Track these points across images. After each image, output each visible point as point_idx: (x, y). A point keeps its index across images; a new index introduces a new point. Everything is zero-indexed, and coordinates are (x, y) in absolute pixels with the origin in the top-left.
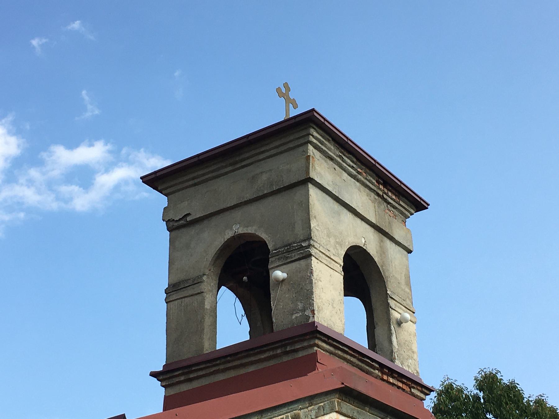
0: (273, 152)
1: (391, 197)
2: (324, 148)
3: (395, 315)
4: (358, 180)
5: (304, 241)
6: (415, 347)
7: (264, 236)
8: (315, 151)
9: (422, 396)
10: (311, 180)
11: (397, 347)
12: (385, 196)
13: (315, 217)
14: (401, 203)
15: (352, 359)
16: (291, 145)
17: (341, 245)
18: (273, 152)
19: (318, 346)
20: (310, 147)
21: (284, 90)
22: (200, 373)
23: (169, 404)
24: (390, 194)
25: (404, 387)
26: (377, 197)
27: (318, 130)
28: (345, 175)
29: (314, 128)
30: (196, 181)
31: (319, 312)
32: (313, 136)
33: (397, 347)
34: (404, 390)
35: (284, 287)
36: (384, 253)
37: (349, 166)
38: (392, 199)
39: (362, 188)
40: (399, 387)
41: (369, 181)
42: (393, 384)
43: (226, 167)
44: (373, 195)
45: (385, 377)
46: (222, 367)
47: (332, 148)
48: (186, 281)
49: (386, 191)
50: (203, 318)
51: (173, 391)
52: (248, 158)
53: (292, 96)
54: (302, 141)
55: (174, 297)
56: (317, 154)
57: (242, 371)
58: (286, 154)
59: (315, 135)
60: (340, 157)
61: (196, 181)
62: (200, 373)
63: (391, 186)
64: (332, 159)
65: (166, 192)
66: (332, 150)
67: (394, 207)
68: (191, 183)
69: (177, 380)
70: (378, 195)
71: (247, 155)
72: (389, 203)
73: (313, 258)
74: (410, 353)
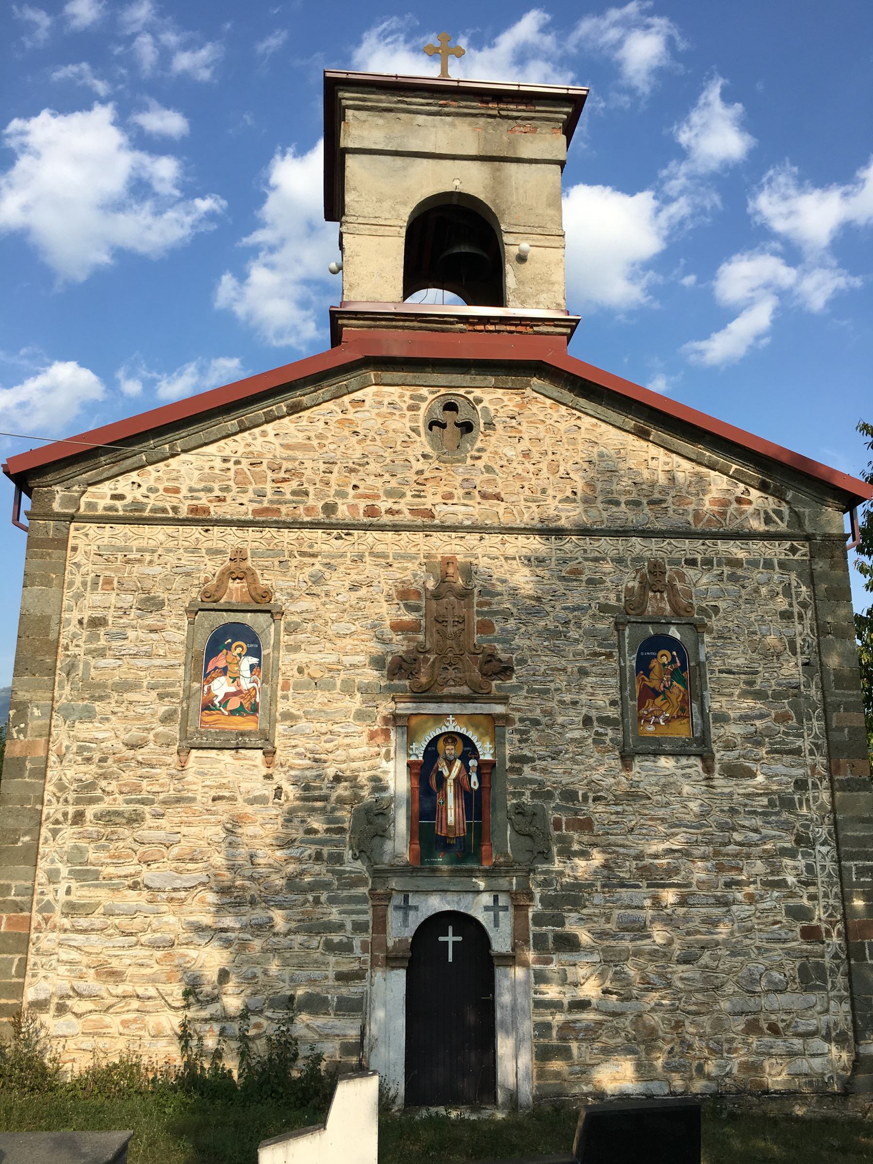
2: (369, 104)
4: (448, 115)
8: (357, 113)
12: (503, 113)
14: (538, 108)
19: (346, 326)
24: (512, 107)
26: (490, 120)
27: (349, 88)
28: (421, 119)
29: (342, 90)
32: (344, 98)
34: (520, 332)
37: (422, 105)
39: (458, 121)
44: (482, 121)
59: (347, 97)
64: (390, 110)
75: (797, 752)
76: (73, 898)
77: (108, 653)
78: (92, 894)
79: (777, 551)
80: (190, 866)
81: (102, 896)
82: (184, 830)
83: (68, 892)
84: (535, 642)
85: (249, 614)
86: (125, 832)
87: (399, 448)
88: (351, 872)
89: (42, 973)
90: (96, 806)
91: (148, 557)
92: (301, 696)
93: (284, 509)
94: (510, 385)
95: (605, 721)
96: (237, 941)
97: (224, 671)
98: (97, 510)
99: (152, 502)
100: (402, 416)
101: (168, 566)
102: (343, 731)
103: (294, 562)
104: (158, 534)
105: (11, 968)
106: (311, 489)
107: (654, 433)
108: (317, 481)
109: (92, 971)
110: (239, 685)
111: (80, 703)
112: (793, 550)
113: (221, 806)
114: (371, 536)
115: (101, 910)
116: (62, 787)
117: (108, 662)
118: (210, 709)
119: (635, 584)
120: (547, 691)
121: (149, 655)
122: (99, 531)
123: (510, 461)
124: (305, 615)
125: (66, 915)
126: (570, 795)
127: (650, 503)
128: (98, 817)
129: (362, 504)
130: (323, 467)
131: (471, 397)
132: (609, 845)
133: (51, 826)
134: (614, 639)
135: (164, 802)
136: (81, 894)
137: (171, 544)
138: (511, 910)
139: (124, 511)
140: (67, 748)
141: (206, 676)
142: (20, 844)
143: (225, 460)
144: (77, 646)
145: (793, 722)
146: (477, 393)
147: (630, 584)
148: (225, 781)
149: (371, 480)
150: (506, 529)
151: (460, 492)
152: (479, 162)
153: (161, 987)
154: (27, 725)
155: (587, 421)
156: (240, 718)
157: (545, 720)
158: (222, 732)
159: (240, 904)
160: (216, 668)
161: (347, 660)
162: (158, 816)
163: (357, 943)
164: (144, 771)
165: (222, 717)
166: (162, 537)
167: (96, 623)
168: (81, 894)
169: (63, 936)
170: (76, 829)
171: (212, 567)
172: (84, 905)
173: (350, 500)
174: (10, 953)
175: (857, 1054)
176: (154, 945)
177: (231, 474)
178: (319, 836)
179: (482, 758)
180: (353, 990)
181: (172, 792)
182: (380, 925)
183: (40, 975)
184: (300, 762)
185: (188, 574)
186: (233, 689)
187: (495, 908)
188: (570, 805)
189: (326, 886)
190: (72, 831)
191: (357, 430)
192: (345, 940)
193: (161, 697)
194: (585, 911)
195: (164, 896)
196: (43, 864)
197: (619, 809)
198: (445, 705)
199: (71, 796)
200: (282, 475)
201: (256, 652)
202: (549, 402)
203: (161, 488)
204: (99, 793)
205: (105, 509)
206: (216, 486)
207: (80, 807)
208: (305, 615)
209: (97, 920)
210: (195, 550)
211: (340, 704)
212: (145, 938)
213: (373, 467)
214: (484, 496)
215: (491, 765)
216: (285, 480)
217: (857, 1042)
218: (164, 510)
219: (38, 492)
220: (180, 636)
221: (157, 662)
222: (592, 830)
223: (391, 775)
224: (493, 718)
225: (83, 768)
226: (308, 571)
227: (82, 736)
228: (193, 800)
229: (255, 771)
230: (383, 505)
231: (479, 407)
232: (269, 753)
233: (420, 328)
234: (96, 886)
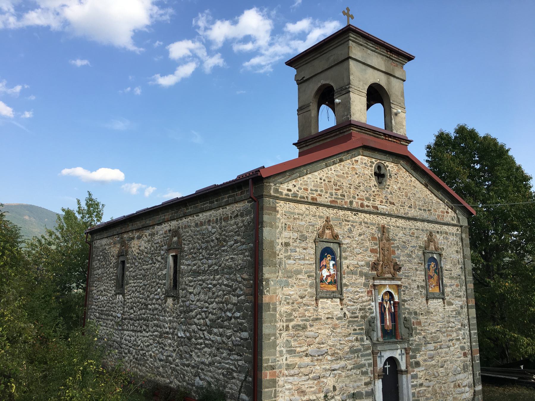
0: (335, 46)
1: (394, 57)
2: (357, 41)
3: (394, 111)
4: (376, 52)
5: (347, 85)
6: (404, 124)
7: (332, 84)
8: (353, 43)
9: (407, 144)
10: (350, 58)
11: (394, 125)
12: (391, 57)
13: (352, 74)
15: (370, 133)
16: (342, 42)
17: (366, 84)
18: (335, 46)
19: (353, 130)
20: (350, 42)
21: (346, 11)
22: (310, 143)
23: (300, 154)
24: (394, 55)
25: (397, 141)
26: (387, 58)
28: (369, 51)
30: (306, 62)
31: (353, 115)
33: (394, 125)
34: (397, 143)
35: (340, 106)
36: (390, 84)
37: (371, 47)
38: (395, 58)
39: (379, 55)
40: (394, 142)
41: (382, 52)
42: (391, 141)
43: (317, 54)
44: (385, 58)
45: (387, 138)
46: (318, 140)
47: (362, 40)
48: (304, 106)
49: (391, 54)
50: (311, 120)
51: (302, 150)
52: (326, 50)
53: (350, 13)
54: (346, 39)
55: (300, 113)
56: (354, 44)
57: (325, 141)
58: (340, 46)
59: (352, 36)
60: (366, 43)
61: (306, 62)
62: (310, 143)
63: (394, 52)
64: (361, 45)
65: (296, 68)
66: (361, 41)
67: (396, 61)
68: (304, 63)
69: (302, 146)
70: (387, 57)
71: (325, 48)
72: (393, 60)
73: (351, 93)
74: (401, 127)
75: (460, 297)
76: (288, 362)
77: (291, 258)
78: (294, 360)
79: (454, 230)
80: (322, 346)
81: (297, 360)
82: (319, 331)
83: (286, 360)
84: (405, 258)
85: (332, 244)
86: (301, 333)
87: (368, 181)
88: (366, 345)
89: (281, 395)
90: (292, 323)
91: (301, 217)
92: (348, 277)
93: (339, 201)
94: (396, 162)
95: (422, 287)
96: (338, 374)
97: (325, 266)
98: (283, 195)
99: (300, 194)
100: (368, 169)
101: (307, 222)
102: (360, 291)
103: (343, 223)
104: (303, 207)
105: (272, 394)
106: (346, 195)
107: (429, 186)
108: (347, 191)
109: (296, 392)
110: (330, 272)
111: (284, 279)
112: (458, 230)
113: (330, 321)
114: (363, 215)
115: (297, 366)
116: (281, 315)
117: (291, 262)
118: (322, 282)
119: (426, 239)
120: (408, 276)
121: (304, 259)
122: (285, 205)
123: (396, 190)
124: (348, 245)
125: (287, 369)
126: (416, 313)
127: (428, 210)
128: (293, 327)
129: (360, 202)
130: (349, 186)
131: (385, 164)
132: (425, 330)
133: (279, 332)
134: (423, 258)
135: (312, 320)
136: (291, 360)
137: (307, 212)
138: (405, 354)
139: (292, 196)
140: (281, 298)
141: (321, 268)
142: (271, 340)
143: (321, 179)
144: (281, 254)
145: (459, 287)
146: (387, 163)
147: (425, 239)
148: (329, 311)
149: (362, 193)
150: (397, 216)
151: (384, 201)
152: (384, 74)
153: (317, 395)
154: (269, 288)
155: (413, 179)
156: (331, 286)
157: (409, 286)
158: (327, 291)
159: (337, 360)
160: (323, 265)
161: (360, 263)
162: (311, 326)
163: (369, 371)
164: (305, 307)
165: (326, 285)
166: (304, 209)
167: (287, 244)
168: (291, 360)
169: (286, 378)
170: (287, 333)
171: (320, 223)
172: (291, 365)
173: (357, 200)
174: (272, 388)
175: (475, 391)
176: (314, 379)
177: (323, 185)
178: (357, 331)
179: (396, 300)
180: (369, 388)
181: (315, 316)
182: (375, 364)
183: (280, 396)
184: (350, 303)
185: (313, 226)
186: (328, 274)
187: (401, 354)
188: (416, 317)
189: (360, 350)
190: (286, 333)
191: (357, 172)
192: (366, 370)
193: (309, 276)
194: (421, 353)
195: (315, 358)
196: (278, 349)
197: (426, 317)
198: (386, 281)
199: (284, 319)
200: (338, 188)
201: (334, 259)
202: (404, 170)
203: (302, 188)
204: (293, 317)
205: (300, 197)
206: (319, 189)
207: (287, 323)
208: (348, 245)
209: (296, 371)
210: (315, 216)
211: (360, 281)
212: (311, 376)
213: (362, 188)
214: (391, 203)
215: (398, 303)
216: (338, 190)
217: (474, 387)
218: (304, 198)
219: (265, 185)
220: (313, 251)
221: (307, 262)
222: (421, 325)
223: (374, 307)
224: (398, 286)
225: (287, 307)
226: (347, 227)
227: (285, 293)
228: (321, 319)
229: (338, 307)
230: (366, 203)
231: (388, 169)
232: (341, 300)
233: (372, 135)
234: (295, 356)
